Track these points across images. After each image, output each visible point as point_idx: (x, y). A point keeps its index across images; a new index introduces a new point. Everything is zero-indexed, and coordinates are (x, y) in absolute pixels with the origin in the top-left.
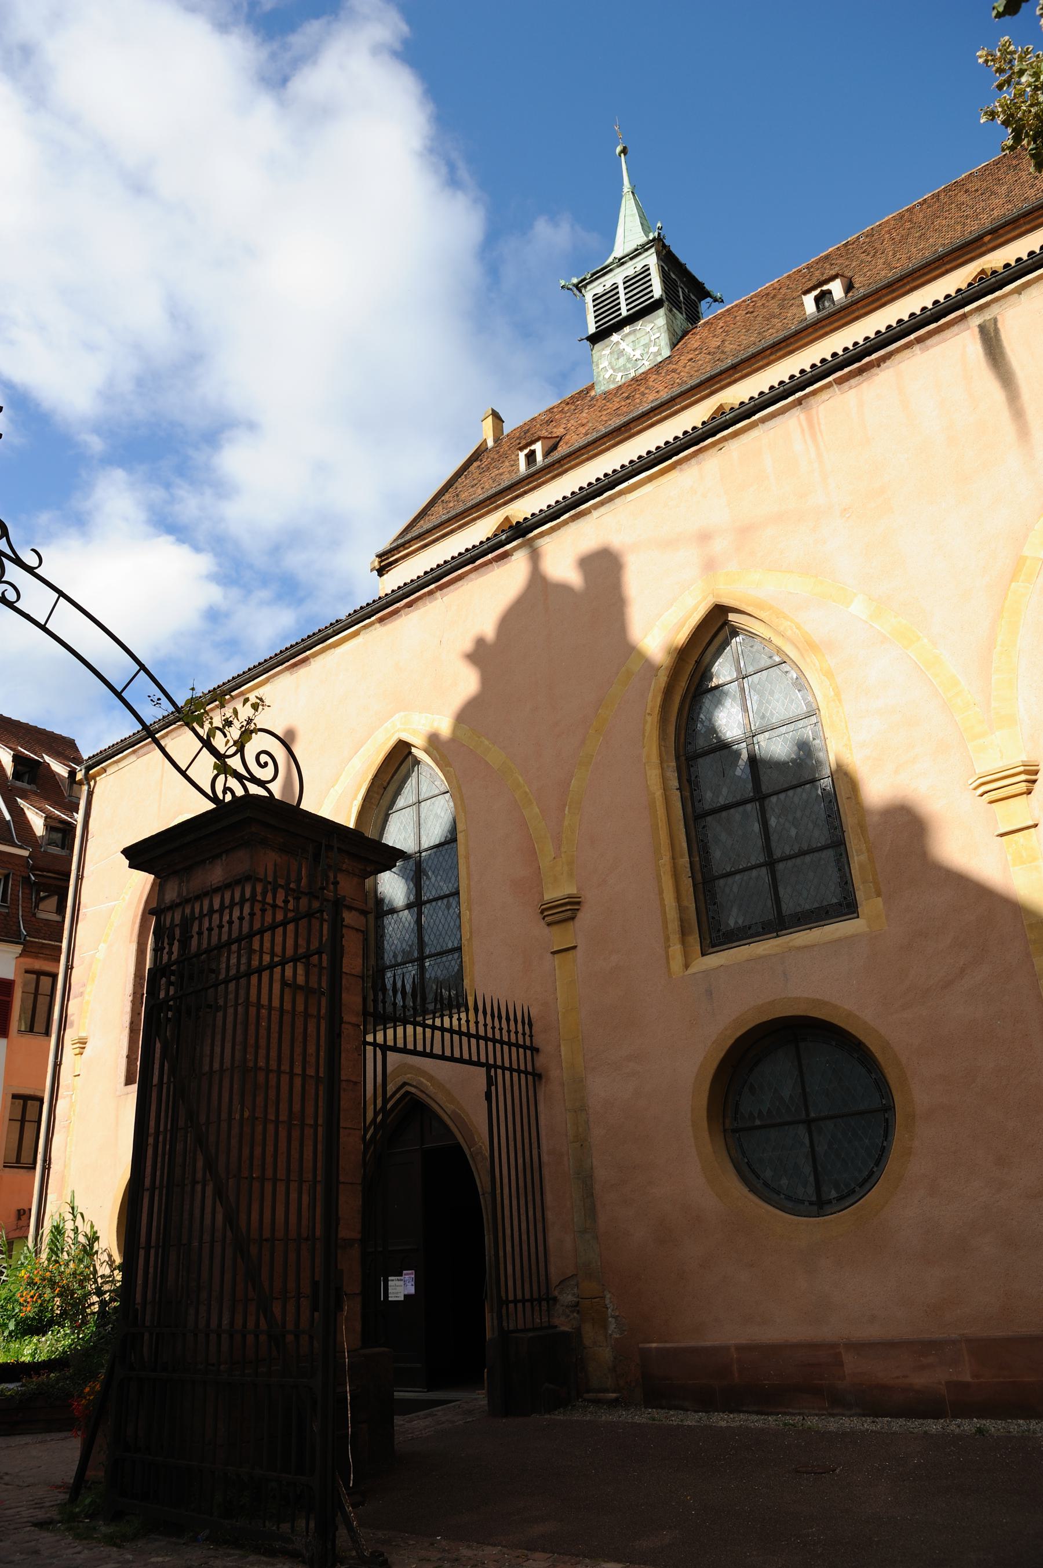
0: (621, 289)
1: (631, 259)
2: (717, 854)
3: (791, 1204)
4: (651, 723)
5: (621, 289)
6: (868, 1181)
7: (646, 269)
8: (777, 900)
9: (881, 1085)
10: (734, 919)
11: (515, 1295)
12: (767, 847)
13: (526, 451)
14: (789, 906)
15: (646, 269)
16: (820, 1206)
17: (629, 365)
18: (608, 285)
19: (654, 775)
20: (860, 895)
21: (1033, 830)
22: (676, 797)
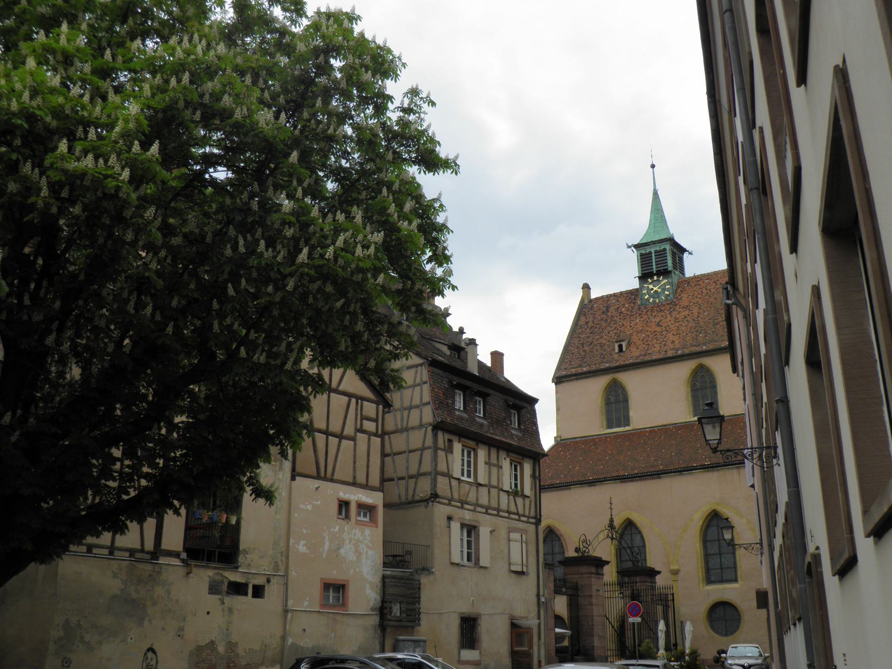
0: (653, 254)
1: (659, 243)
2: (710, 564)
3: (721, 634)
4: (698, 533)
5: (653, 254)
6: (735, 631)
7: (665, 250)
8: (722, 576)
9: (739, 615)
10: (713, 579)
11: (529, 513)
12: (721, 565)
13: (618, 344)
14: (724, 578)
15: (665, 250)
16: (726, 635)
17: (656, 296)
18: (648, 251)
19: (698, 545)
20: (739, 579)
21: (742, 397)
22: (702, 550)
